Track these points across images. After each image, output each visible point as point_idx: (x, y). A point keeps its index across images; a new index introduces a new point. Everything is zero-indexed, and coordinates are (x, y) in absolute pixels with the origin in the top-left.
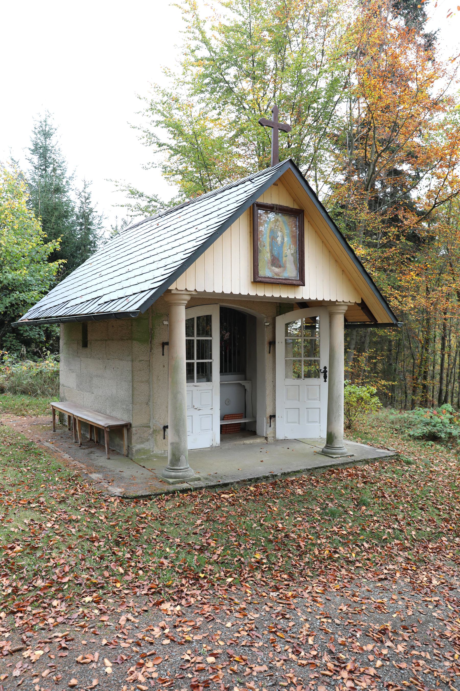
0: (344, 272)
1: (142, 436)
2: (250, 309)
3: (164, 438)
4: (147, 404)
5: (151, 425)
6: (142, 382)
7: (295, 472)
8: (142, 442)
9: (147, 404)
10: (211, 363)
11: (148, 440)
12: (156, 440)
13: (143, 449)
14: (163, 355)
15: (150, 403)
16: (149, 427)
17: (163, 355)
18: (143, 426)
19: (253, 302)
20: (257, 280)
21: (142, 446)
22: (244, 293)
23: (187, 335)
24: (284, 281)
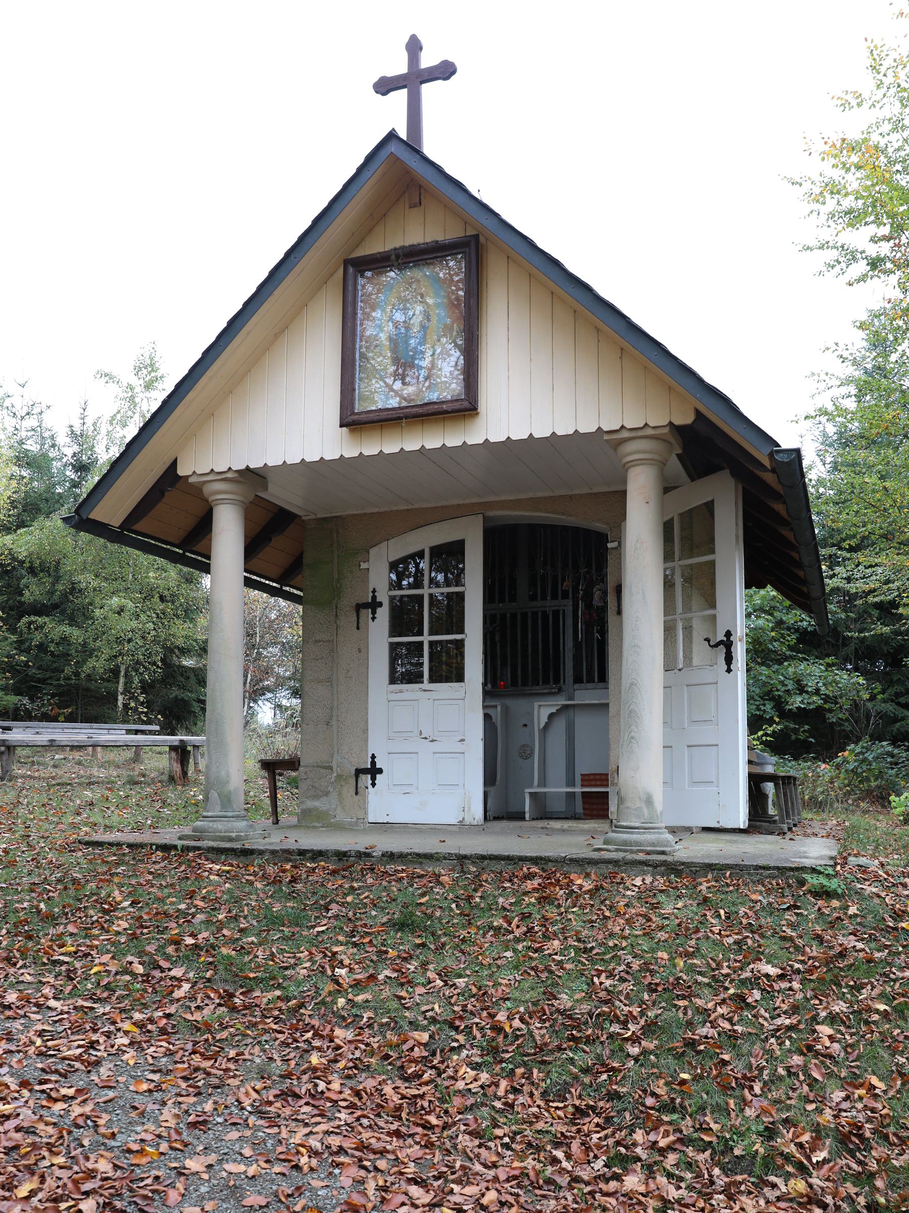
0: (281, 331)
1: (316, 785)
2: (563, 514)
3: (357, 793)
4: (328, 723)
5: (334, 765)
6: (320, 681)
7: (418, 855)
8: (316, 797)
9: (328, 723)
10: (391, 635)
11: (327, 794)
12: (340, 794)
13: (316, 809)
14: (358, 628)
15: (334, 722)
16: (331, 768)
17: (358, 628)
18: (322, 767)
19: (571, 497)
20: (353, 421)
21: (317, 803)
22: (331, 455)
23: (461, 597)
24: (420, 410)
